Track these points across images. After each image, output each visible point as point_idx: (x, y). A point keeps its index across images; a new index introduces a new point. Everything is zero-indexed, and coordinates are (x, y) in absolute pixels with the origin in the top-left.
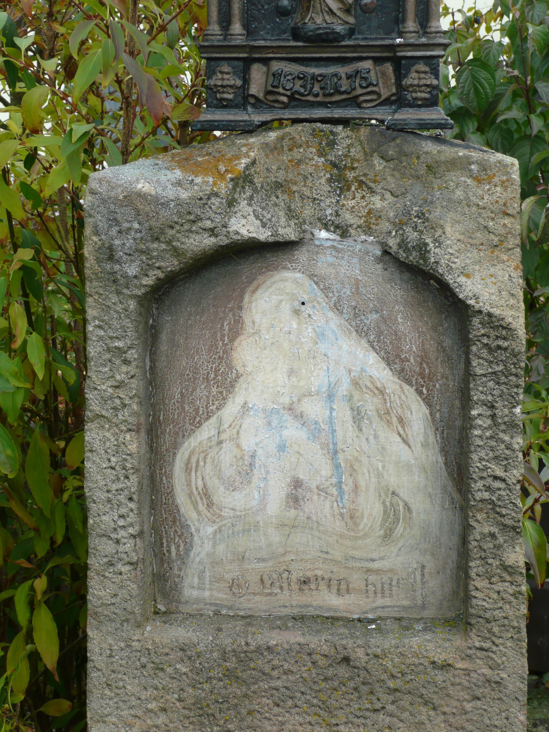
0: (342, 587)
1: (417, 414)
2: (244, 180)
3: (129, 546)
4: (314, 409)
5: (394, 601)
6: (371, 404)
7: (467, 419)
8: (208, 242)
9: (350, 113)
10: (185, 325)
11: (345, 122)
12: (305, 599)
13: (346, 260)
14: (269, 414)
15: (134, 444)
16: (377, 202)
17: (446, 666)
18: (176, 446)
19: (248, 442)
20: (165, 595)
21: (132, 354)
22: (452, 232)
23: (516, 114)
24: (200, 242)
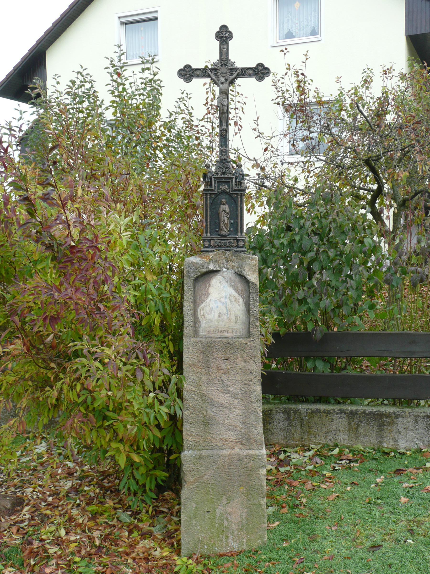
0: (228, 332)
1: (241, 301)
2: (211, 260)
3: (191, 323)
4: (223, 300)
5: (238, 334)
6: (233, 299)
7: (249, 301)
8: (205, 270)
9: (229, 249)
10: (200, 285)
11: (228, 250)
12: (222, 334)
13: (228, 274)
15: (192, 305)
16: (234, 264)
17: (246, 344)
18: (198, 307)
19: (211, 306)
20: (196, 334)
21: (192, 289)
22: (246, 269)
23: (268, 248)
24: (204, 270)
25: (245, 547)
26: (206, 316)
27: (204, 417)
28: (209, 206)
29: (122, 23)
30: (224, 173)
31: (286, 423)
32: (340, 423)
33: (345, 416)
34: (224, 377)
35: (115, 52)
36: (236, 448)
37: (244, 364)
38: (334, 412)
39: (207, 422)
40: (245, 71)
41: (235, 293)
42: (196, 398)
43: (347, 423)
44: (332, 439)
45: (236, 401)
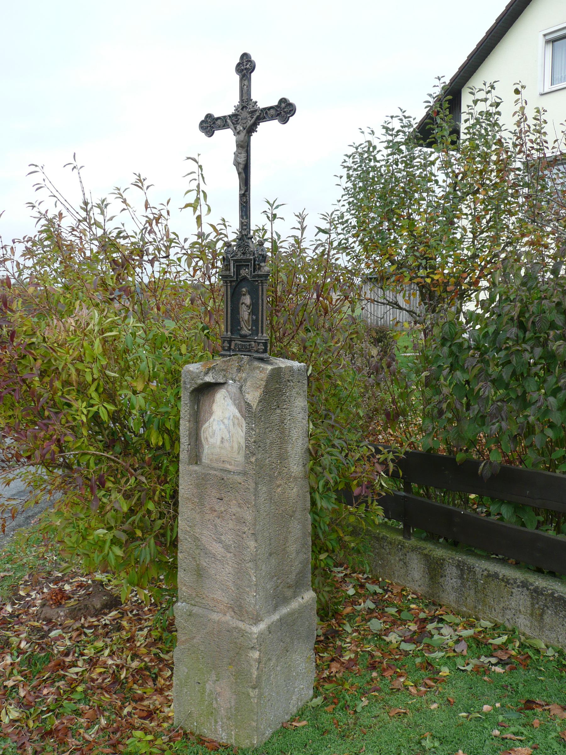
4: (226, 421)
6: (236, 421)
14: (218, 421)
19: (214, 427)
25: (233, 741)
26: (209, 439)
27: (198, 565)
28: (229, 296)
29: (547, 42)
30: (244, 254)
31: (459, 581)
32: (520, 600)
33: (528, 593)
34: (218, 521)
35: (434, 86)
36: (228, 614)
37: (239, 510)
38: (515, 583)
39: (200, 573)
40: (266, 113)
41: (238, 415)
42: (189, 540)
43: (529, 603)
44: (511, 621)
45: (229, 555)
